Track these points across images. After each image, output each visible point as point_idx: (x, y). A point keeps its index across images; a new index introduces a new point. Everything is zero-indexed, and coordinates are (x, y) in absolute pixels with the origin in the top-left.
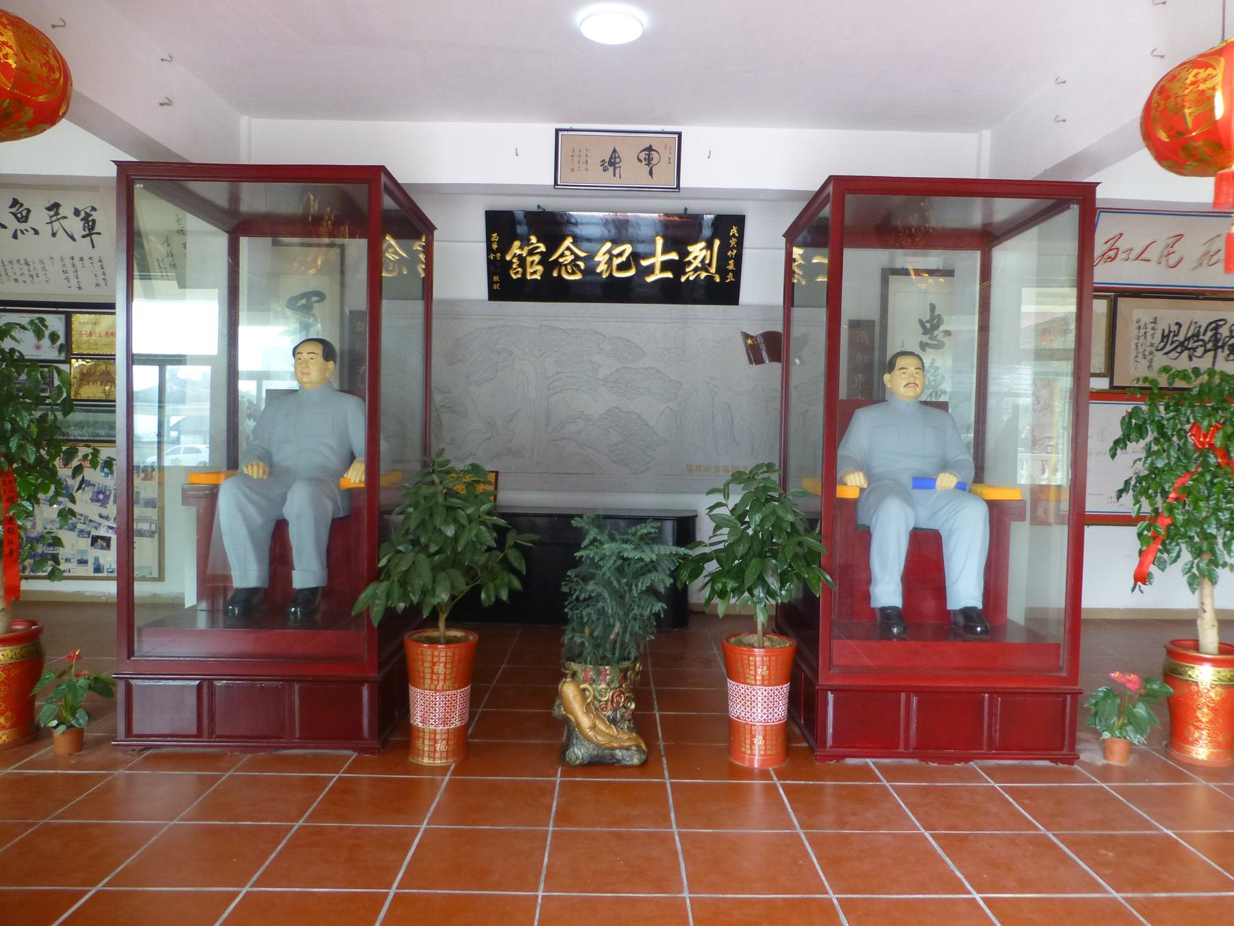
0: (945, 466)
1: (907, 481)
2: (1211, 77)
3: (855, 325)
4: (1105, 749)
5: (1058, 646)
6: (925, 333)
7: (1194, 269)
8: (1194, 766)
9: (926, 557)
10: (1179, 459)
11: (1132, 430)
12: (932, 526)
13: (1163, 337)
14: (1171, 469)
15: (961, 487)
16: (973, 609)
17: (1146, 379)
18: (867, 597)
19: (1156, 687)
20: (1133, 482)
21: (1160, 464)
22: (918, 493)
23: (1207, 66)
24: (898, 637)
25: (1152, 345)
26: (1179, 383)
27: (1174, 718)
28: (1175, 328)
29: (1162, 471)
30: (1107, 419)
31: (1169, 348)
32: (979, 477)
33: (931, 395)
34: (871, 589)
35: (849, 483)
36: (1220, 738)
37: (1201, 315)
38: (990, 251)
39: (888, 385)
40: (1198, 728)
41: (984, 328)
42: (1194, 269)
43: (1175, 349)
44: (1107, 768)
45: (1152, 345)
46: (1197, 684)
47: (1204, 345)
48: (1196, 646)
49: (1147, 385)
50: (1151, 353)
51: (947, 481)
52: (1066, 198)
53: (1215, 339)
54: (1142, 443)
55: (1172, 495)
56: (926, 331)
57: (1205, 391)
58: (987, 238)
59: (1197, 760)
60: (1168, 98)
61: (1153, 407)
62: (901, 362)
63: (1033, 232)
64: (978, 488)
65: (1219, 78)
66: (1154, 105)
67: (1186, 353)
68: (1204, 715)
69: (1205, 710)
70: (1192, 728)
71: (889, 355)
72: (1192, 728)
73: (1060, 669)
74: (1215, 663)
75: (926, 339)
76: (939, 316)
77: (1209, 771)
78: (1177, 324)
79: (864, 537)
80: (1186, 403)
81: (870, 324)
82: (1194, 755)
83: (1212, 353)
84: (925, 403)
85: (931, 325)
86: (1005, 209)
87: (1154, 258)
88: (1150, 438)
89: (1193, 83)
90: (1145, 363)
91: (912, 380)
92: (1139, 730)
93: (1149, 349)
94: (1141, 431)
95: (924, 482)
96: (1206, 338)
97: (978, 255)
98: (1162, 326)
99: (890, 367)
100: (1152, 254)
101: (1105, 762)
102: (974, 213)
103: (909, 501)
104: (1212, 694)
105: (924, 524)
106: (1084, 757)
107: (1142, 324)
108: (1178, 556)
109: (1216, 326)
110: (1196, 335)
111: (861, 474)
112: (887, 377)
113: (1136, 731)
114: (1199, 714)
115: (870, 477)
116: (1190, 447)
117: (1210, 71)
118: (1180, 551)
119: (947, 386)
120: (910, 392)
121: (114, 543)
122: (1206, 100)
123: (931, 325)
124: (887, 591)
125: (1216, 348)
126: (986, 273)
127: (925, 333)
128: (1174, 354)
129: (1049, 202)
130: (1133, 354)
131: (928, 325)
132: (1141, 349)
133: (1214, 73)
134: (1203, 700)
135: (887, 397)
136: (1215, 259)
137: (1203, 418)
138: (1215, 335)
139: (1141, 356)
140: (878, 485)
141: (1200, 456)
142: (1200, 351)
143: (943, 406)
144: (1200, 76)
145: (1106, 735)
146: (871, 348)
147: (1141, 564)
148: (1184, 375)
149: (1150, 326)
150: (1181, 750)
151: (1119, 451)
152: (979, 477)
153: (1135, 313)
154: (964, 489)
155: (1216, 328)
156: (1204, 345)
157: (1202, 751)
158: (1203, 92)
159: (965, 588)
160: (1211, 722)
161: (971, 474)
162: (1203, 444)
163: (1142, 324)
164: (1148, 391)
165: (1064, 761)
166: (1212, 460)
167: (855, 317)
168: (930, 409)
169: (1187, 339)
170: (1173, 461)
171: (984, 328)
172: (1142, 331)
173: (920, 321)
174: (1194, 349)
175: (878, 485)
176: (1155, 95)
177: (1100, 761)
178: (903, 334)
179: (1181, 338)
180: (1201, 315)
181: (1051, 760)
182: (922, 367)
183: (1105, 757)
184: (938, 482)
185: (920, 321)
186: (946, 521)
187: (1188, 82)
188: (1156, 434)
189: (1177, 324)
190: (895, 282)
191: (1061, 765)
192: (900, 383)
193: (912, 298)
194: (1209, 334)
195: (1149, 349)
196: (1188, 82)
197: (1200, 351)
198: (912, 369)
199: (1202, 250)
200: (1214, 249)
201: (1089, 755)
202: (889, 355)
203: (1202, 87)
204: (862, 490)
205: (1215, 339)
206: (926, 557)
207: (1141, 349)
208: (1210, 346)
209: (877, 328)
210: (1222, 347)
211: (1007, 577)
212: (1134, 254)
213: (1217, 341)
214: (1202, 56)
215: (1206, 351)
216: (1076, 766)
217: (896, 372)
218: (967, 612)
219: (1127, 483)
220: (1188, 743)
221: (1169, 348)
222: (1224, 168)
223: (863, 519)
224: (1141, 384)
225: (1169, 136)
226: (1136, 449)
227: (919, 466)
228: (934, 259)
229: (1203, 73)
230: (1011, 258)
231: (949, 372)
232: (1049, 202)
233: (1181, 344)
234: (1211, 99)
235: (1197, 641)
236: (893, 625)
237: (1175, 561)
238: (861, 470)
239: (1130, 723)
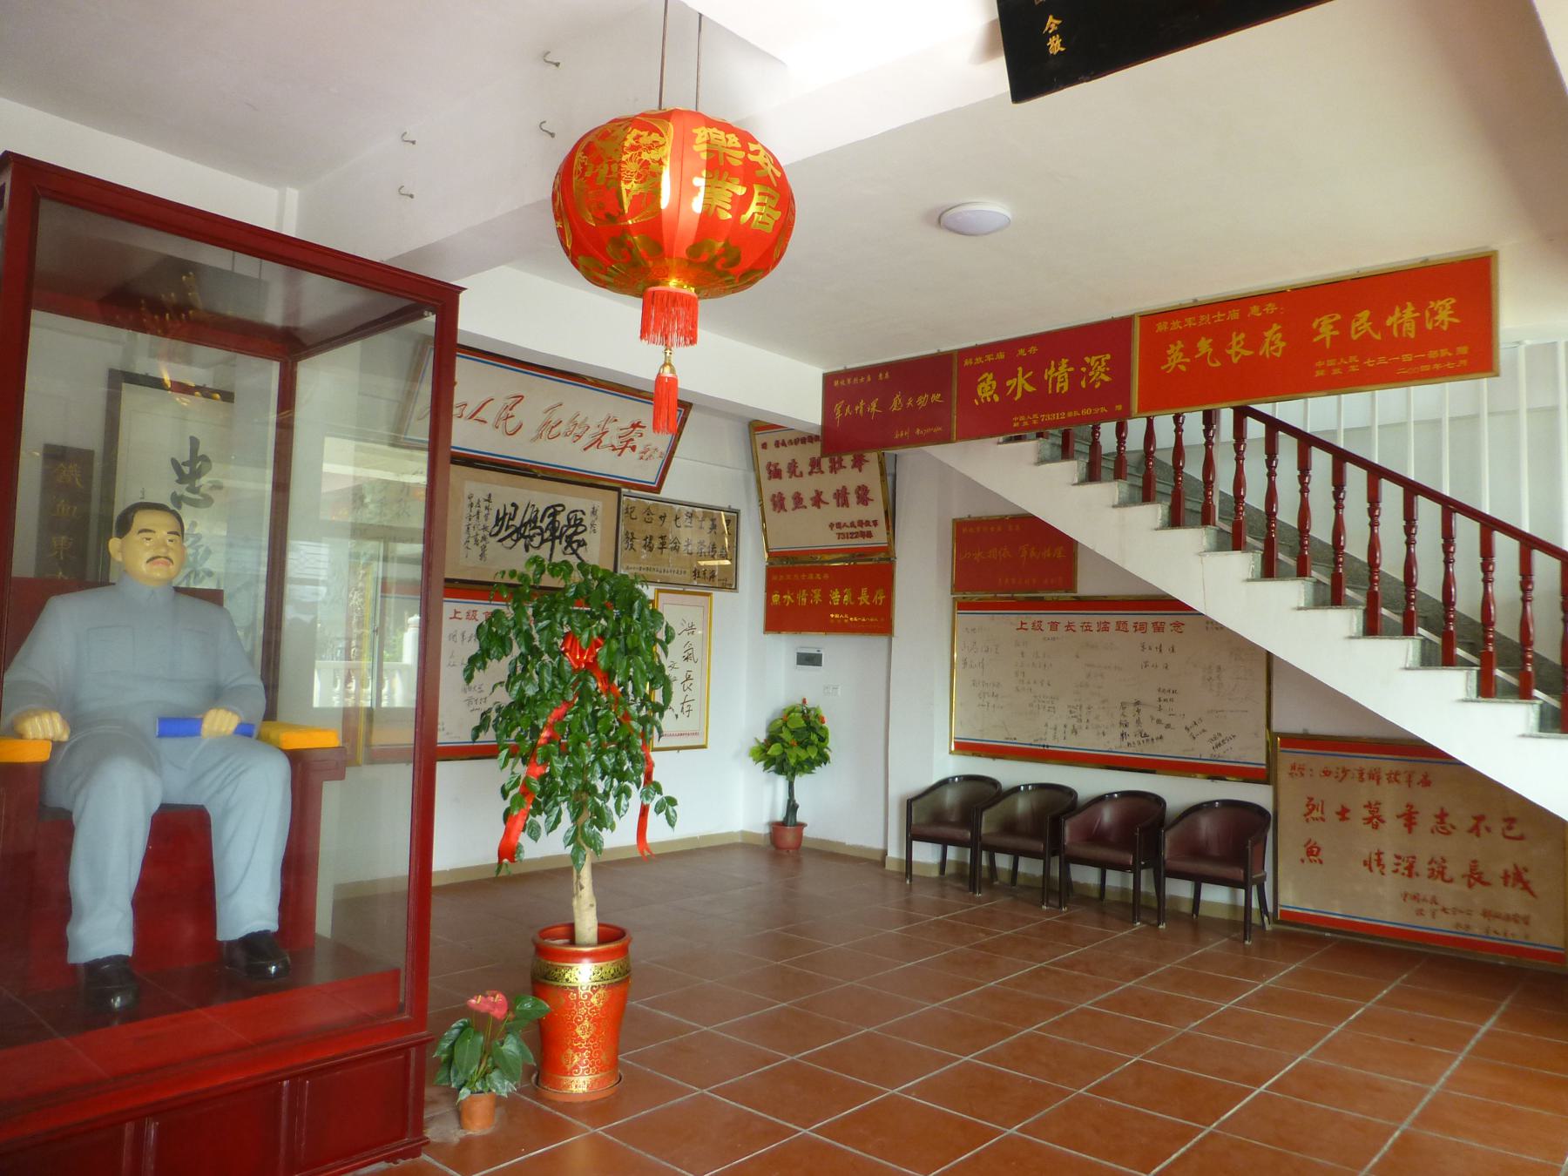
0: (217, 695)
1: (152, 728)
2: (655, 145)
3: (56, 455)
4: (460, 1114)
5: (397, 972)
6: (180, 481)
7: (534, 440)
8: (571, 1107)
9: (181, 850)
10: (553, 685)
11: (491, 641)
12: (193, 800)
13: (498, 520)
14: (544, 699)
15: (244, 731)
16: (263, 935)
17: (513, 574)
18: (61, 944)
19: (528, 1006)
20: (493, 715)
21: (531, 691)
22: (169, 746)
23: (652, 130)
24: (128, 1015)
25: (485, 528)
26: (547, 581)
27: (547, 1047)
28: (510, 510)
29: (532, 701)
30: (462, 623)
31: (503, 534)
32: (270, 714)
33: (188, 576)
34: (69, 929)
35: (30, 734)
36: (604, 1057)
37: (539, 496)
38: (294, 365)
39: (119, 558)
40: (577, 1050)
41: (282, 486)
42: (534, 440)
43: (510, 535)
44: (466, 1143)
45: (485, 528)
46: (575, 989)
47: (542, 534)
48: (570, 934)
49: (515, 581)
50: (484, 538)
51: (221, 722)
52: (410, 300)
53: (553, 526)
54: (506, 661)
55: (545, 734)
56: (182, 478)
57: (583, 594)
58: (289, 346)
59: (577, 1094)
60: (598, 161)
61: (519, 609)
62: (142, 520)
63: (354, 349)
64: (272, 731)
65: (668, 149)
66: (577, 167)
67: (522, 541)
68: (584, 1030)
69: (586, 1023)
70: (570, 1052)
71: (118, 509)
72: (570, 1052)
73: (399, 1009)
74: (595, 957)
75: (182, 490)
76: (205, 459)
77: (596, 1110)
78: (513, 505)
79: (62, 829)
80: (562, 607)
81: (84, 457)
82: (574, 1089)
83: (549, 544)
84: (177, 590)
85: (190, 469)
86: (322, 298)
87: (491, 420)
88: (516, 651)
89: (633, 148)
90: (477, 551)
91: (162, 551)
92: (508, 1073)
93: (481, 533)
94: (504, 645)
95: (180, 725)
96: (544, 525)
97: (274, 369)
98: (496, 505)
99: (124, 526)
100: (489, 414)
101: (461, 1134)
102: (275, 297)
103: (151, 761)
104: (594, 1000)
105: (178, 798)
106: (431, 1133)
107: (474, 500)
108: (558, 821)
109: (554, 510)
110: (533, 520)
111: (57, 718)
112: (114, 544)
113: (503, 1078)
114: (579, 1031)
115: (74, 721)
116: (566, 668)
117: (655, 136)
118: (560, 812)
119: (215, 563)
120: (159, 572)
121: (1179, 411)
122: (650, 175)
123: (190, 469)
124: (104, 928)
125: (553, 539)
126: (287, 399)
127: (180, 481)
128: (509, 542)
129: (399, 303)
130: (464, 537)
131: (186, 470)
132: (473, 533)
133: (661, 141)
134: (583, 1011)
135: (113, 577)
136: (555, 431)
137: (583, 629)
138: (553, 522)
139: (472, 540)
140: (92, 736)
141: (579, 679)
142: (537, 540)
143: (215, 597)
144: (642, 141)
145: (465, 1093)
146: (86, 497)
147: (507, 834)
148: (556, 569)
149: (484, 504)
150: (557, 1085)
151: (476, 673)
152: (270, 714)
153: (468, 486)
154: (250, 735)
155: (554, 515)
156: (542, 534)
157: (580, 1083)
158: (646, 163)
159: (248, 903)
160: (593, 1037)
161: (260, 703)
162: (578, 663)
163: (474, 500)
164: (516, 591)
165: (404, 1155)
166: (593, 685)
167: (56, 440)
168: (184, 599)
169: (523, 525)
170: (547, 686)
171: (282, 486)
172: (475, 510)
173: (174, 462)
174: (531, 538)
175: (92, 736)
176: (579, 154)
177: (455, 1135)
178: (144, 471)
179: (517, 522)
180: (539, 496)
181: (388, 1159)
182: (180, 532)
183: (461, 1127)
184: (206, 726)
185: (174, 462)
186: (218, 792)
187: (627, 144)
188: (523, 649)
189: (513, 505)
190: (132, 397)
191: (401, 1162)
192: (139, 555)
193: (155, 432)
194: (547, 520)
195: (481, 533)
196: (627, 144)
197: (537, 540)
198: (162, 533)
199: (543, 418)
200: (554, 420)
201: (441, 1129)
202: (118, 509)
203: (645, 156)
204: (57, 745)
205: (553, 526)
206: (181, 850)
207: (473, 533)
208: (547, 535)
209: (98, 465)
210: (560, 538)
211: (316, 876)
212: (468, 411)
213: (554, 530)
214: (643, 115)
215: (543, 541)
216: (424, 1157)
217: (133, 536)
218: (253, 942)
219: (485, 716)
220: (566, 1074)
221: (503, 534)
222: (656, 284)
223: (57, 795)
224: (507, 579)
225: (595, 218)
226: (499, 668)
227: (180, 699)
228: (201, 364)
229: (646, 138)
230: (324, 382)
231: (221, 547)
232: (399, 303)
233: (517, 530)
234: (657, 175)
235: (572, 926)
236: (112, 995)
237: (554, 828)
238: (58, 710)
239: (495, 1067)
